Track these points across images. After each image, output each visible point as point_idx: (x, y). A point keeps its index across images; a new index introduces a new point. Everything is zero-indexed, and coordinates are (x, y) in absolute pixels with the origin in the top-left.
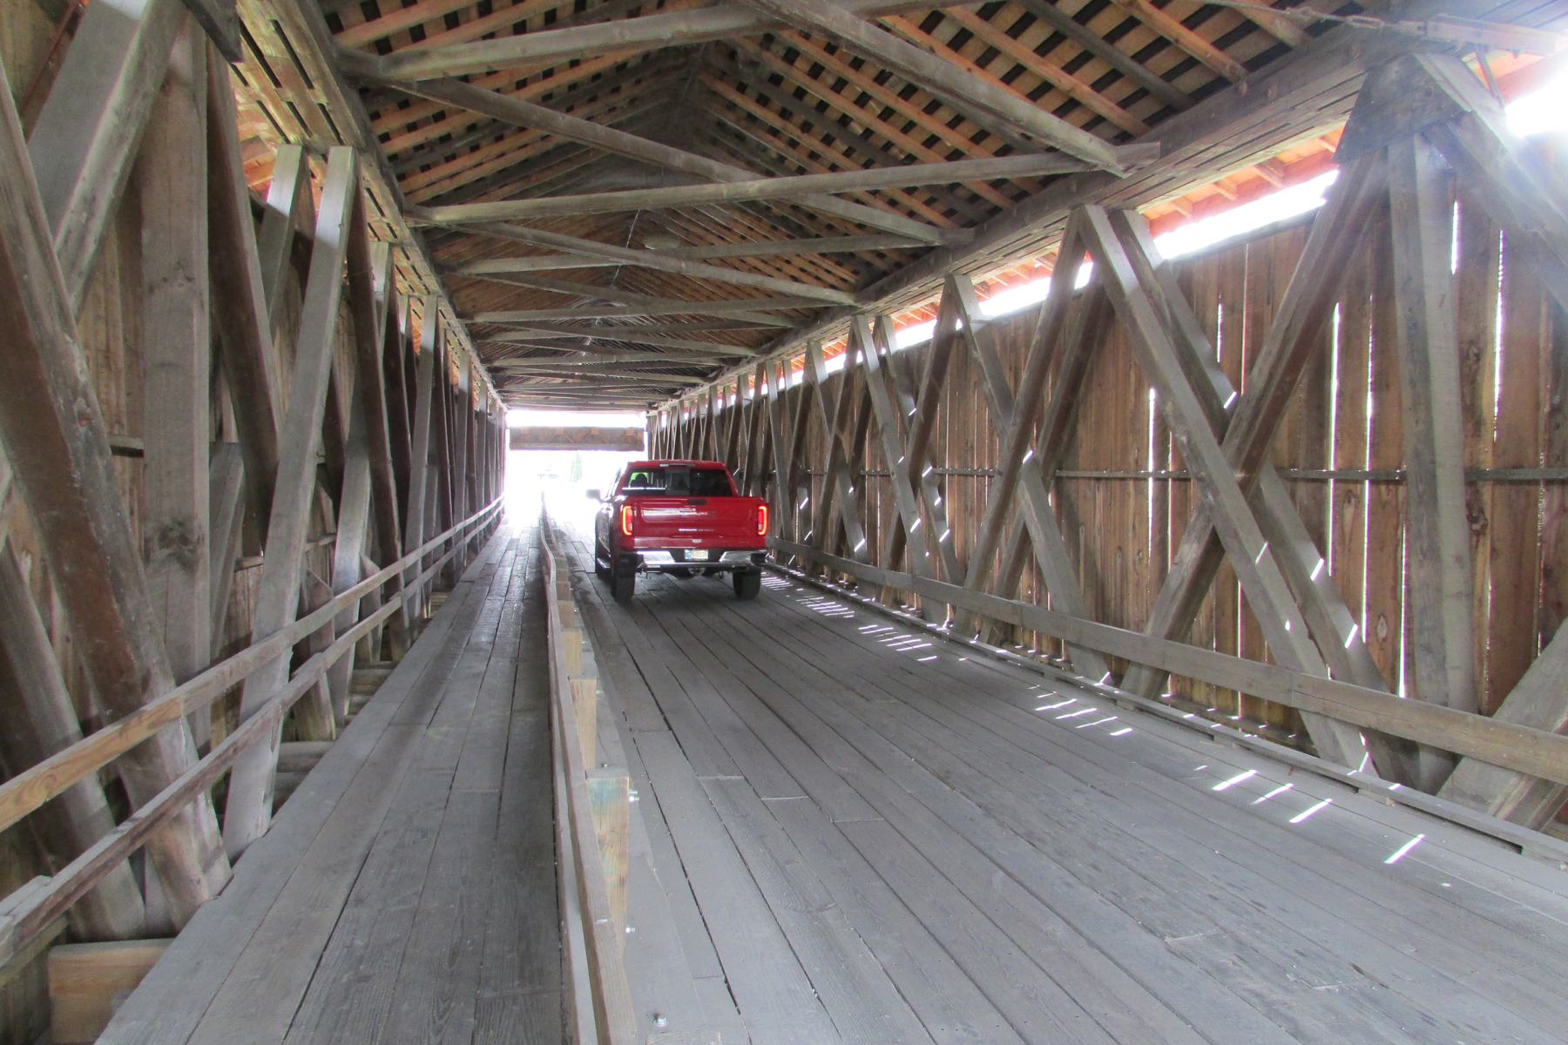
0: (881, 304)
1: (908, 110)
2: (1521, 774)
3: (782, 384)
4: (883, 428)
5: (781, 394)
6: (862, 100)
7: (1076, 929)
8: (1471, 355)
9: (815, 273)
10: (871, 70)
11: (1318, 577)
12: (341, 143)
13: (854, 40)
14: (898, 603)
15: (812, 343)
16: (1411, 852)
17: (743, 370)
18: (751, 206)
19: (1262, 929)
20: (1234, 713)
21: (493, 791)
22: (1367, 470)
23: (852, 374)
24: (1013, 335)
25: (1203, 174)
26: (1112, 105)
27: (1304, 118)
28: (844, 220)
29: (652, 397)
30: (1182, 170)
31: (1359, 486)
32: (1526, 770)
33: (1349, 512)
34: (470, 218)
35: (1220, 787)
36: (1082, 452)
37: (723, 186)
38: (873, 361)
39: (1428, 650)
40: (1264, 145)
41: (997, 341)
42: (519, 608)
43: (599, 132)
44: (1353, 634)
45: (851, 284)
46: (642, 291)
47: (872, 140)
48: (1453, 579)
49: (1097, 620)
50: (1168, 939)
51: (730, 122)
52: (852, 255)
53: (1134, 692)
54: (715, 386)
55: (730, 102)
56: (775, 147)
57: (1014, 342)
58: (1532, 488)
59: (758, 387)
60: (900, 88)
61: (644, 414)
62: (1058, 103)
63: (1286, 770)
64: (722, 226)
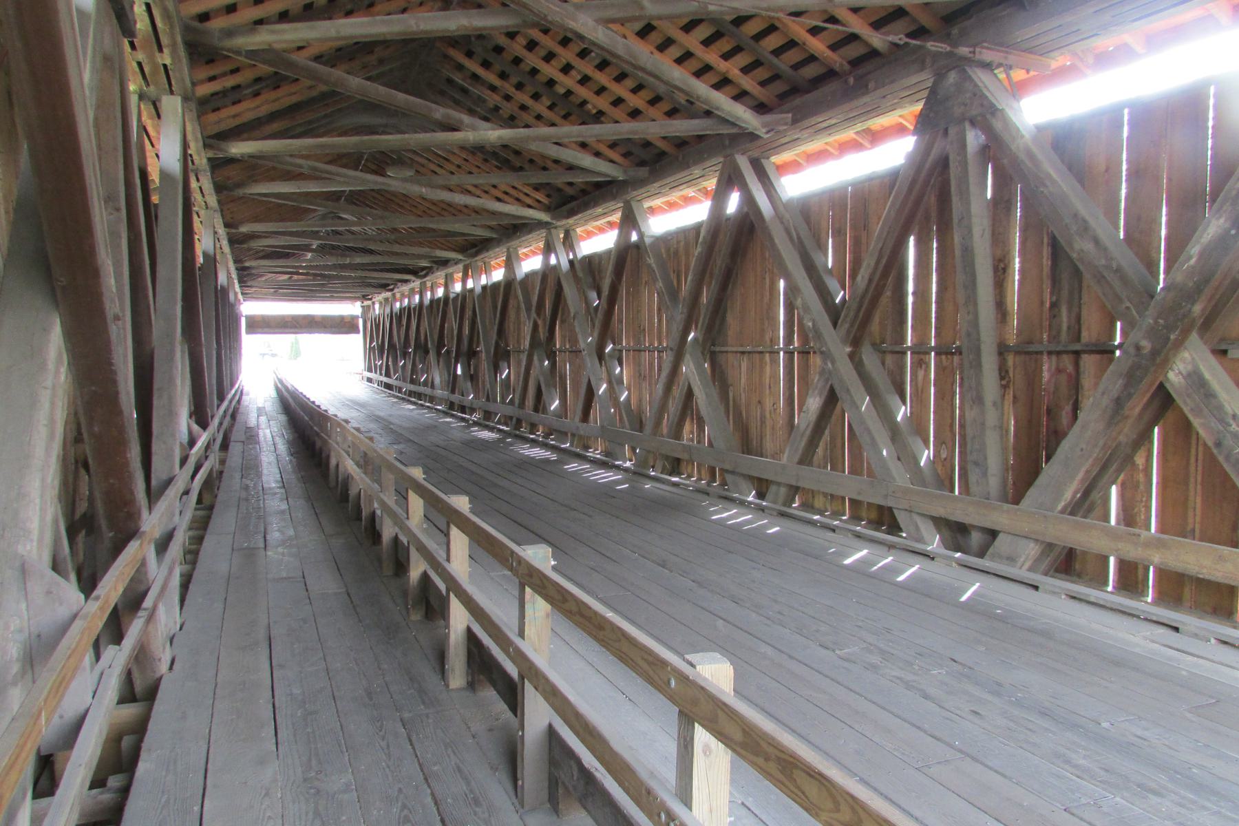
0: (571, 221)
1: (602, 78)
2: (1036, 541)
3: (484, 280)
4: (574, 316)
5: (484, 288)
6: (567, 69)
7: (780, 650)
8: (1000, 269)
9: (517, 196)
10: (576, 47)
11: (902, 418)
12: (172, 93)
13: (595, 40)
14: (586, 448)
15: (511, 249)
16: (975, 593)
17: (450, 270)
18: (479, 150)
19: (892, 642)
20: (844, 514)
21: (340, 591)
22: (933, 345)
23: (547, 275)
24: (675, 246)
25: (818, 137)
26: (755, 84)
27: (890, 103)
28: (543, 157)
29: (368, 290)
30: (805, 134)
31: (927, 356)
32: (1041, 538)
33: (921, 373)
34: (261, 152)
35: (848, 561)
36: (730, 333)
37: (469, 133)
38: (565, 265)
39: (976, 464)
40: (863, 119)
41: (663, 251)
42: (291, 461)
43: (355, 83)
44: (925, 456)
45: (545, 204)
46: (368, 206)
47: (572, 98)
48: (991, 417)
49: (743, 453)
50: (837, 652)
51: (458, 78)
52: (548, 184)
53: (775, 502)
54: (425, 282)
55: (460, 64)
56: (493, 99)
57: (676, 253)
58: (1039, 356)
59: (464, 282)
60: (597, 62)
61: (358, 304)
62: (715, 80)
63: (886, 549)
64: (440, 156)
